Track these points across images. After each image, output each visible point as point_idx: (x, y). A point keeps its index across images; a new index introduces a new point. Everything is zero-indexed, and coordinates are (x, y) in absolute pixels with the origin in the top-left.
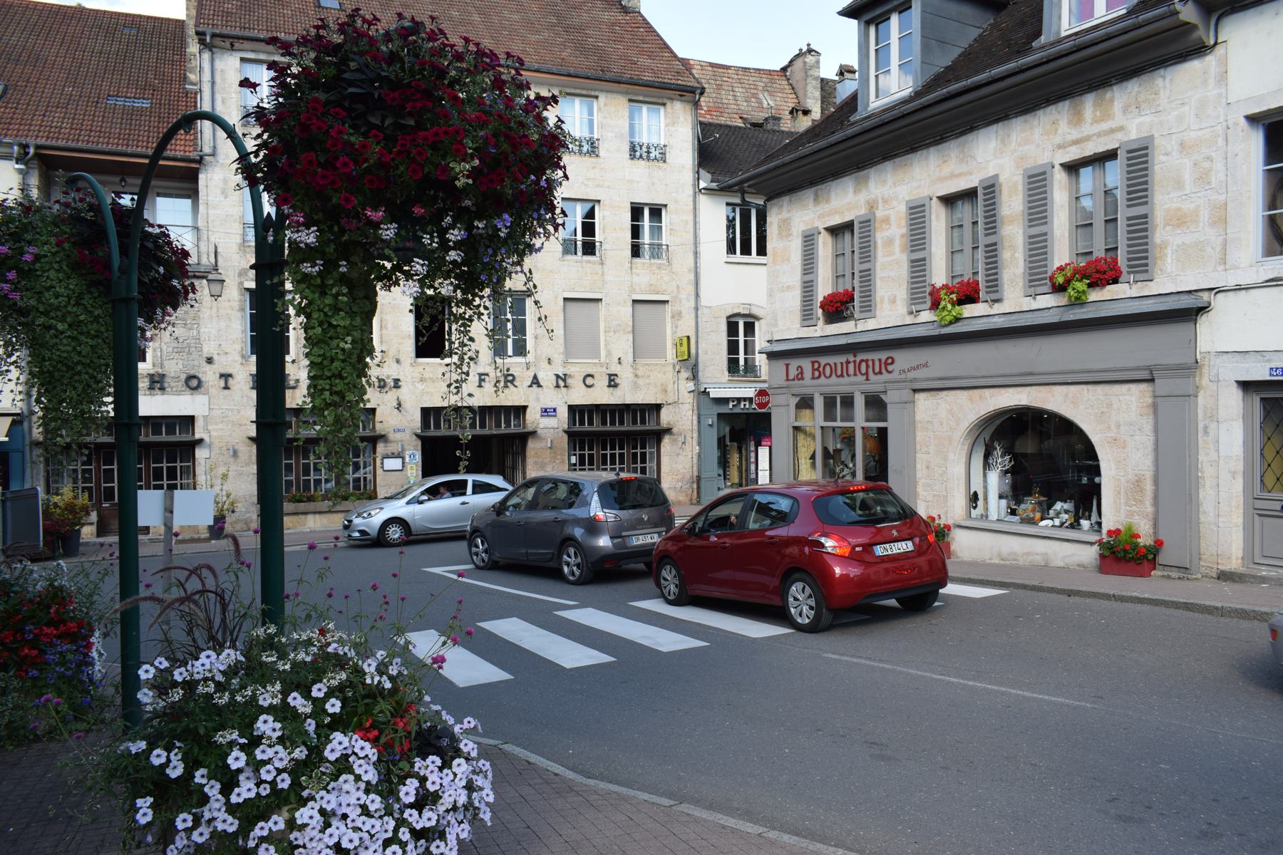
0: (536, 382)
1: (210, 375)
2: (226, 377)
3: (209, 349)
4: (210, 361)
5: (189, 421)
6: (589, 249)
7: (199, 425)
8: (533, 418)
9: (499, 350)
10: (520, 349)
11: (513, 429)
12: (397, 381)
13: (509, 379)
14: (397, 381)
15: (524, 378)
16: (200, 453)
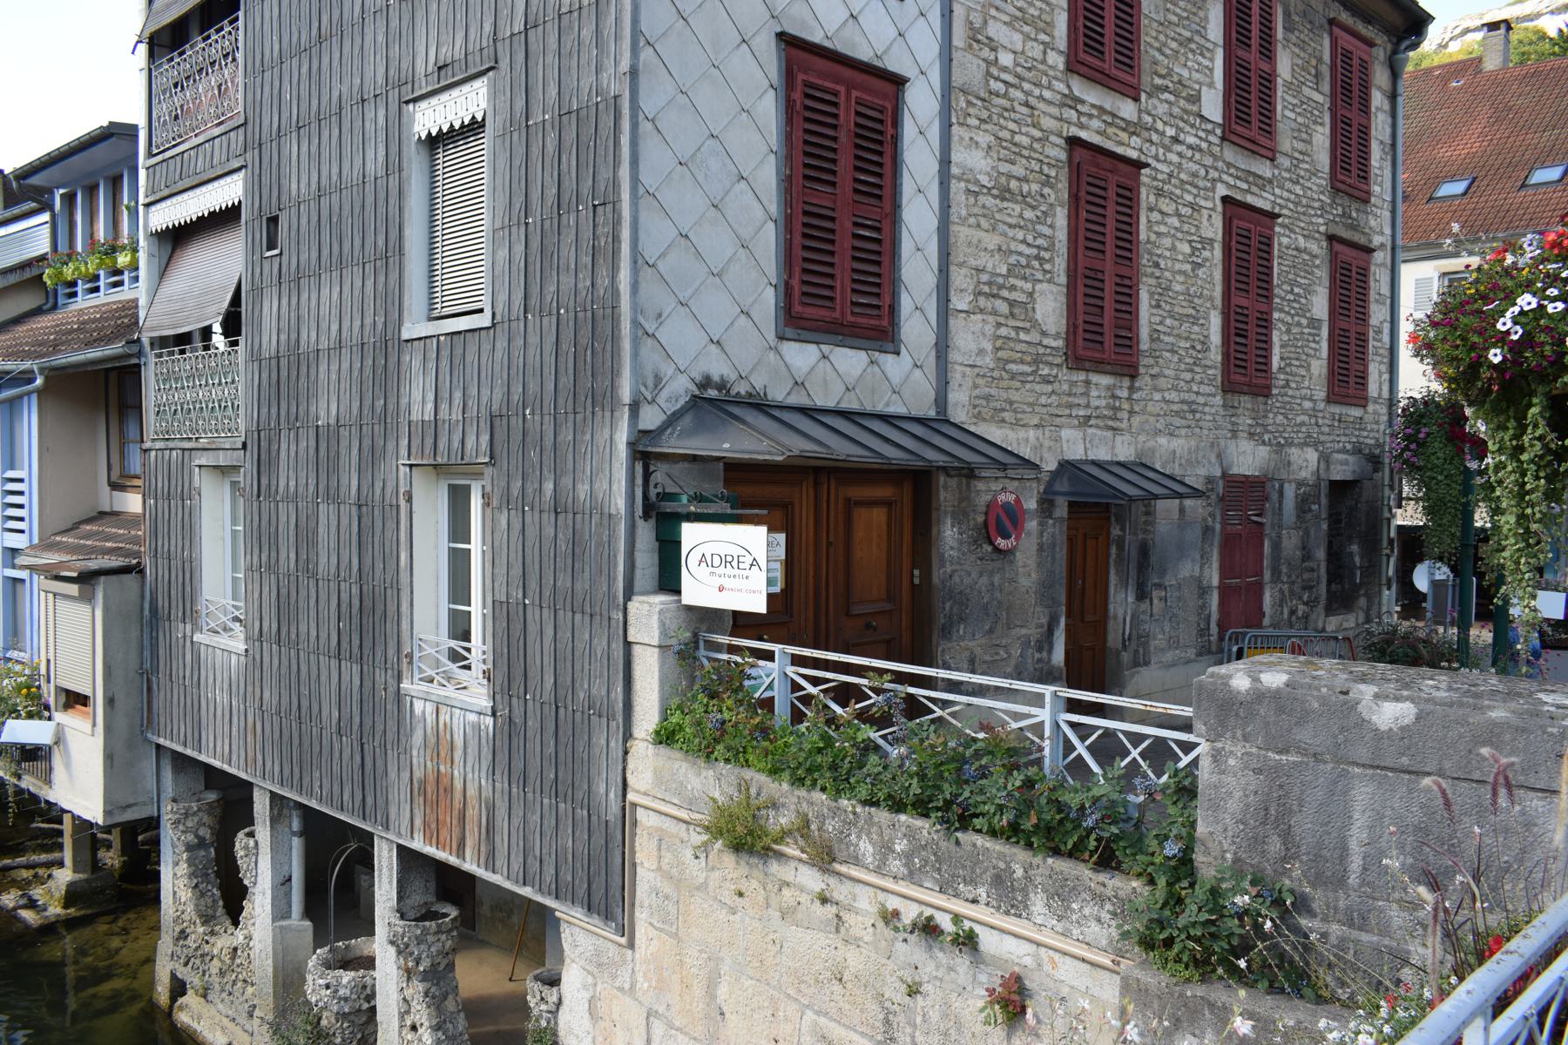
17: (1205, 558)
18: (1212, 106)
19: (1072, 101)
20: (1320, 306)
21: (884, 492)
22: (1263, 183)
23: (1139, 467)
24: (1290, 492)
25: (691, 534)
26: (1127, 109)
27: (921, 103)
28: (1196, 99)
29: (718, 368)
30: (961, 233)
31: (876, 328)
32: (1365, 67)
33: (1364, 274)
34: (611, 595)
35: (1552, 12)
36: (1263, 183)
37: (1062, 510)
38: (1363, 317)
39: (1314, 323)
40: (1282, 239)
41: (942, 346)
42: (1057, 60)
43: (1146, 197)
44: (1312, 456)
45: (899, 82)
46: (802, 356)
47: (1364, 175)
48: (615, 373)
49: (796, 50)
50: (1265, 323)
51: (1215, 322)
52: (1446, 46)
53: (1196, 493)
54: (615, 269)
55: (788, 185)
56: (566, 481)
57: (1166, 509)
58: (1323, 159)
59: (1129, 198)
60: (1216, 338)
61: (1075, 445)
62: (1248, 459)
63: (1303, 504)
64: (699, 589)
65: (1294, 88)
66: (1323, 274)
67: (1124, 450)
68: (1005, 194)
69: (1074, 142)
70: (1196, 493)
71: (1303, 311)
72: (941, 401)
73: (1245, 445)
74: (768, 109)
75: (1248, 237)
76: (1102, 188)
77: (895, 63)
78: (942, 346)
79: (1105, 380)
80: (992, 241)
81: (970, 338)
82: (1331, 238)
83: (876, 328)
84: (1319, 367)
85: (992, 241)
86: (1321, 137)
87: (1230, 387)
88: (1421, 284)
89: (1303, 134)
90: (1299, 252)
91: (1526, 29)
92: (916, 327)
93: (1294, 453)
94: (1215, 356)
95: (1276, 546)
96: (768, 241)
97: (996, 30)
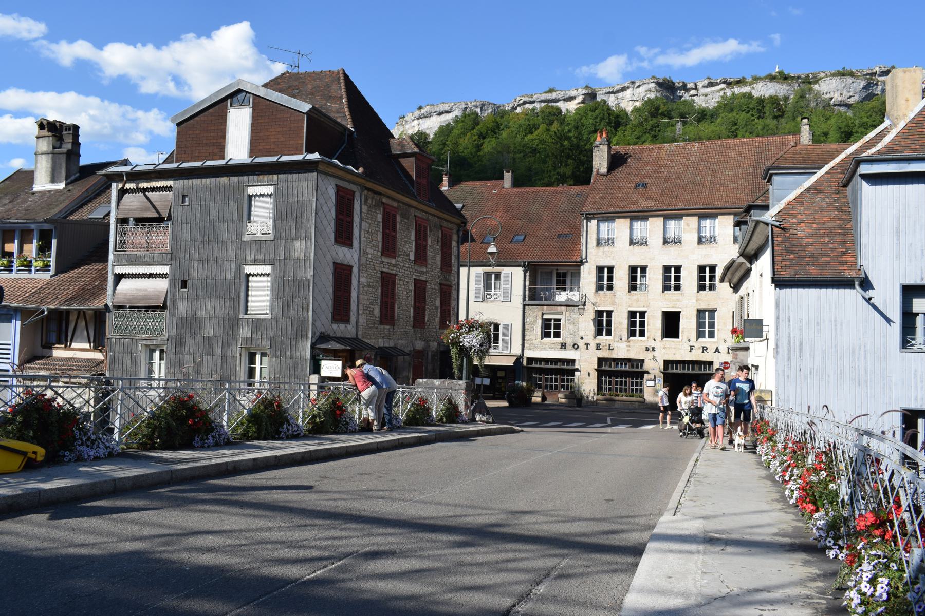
0: (717, 350)
1: (581, 344)
2: (587, 345)
3: (582, 334)
4: (582, 338)
5: (573, 361)
6: (677, 288)
7: (577, 362)
8: (648, 365)
9: (700, 334)
10: (712, 335)
11: (707, 372)
12: (653, 348)
13: (704, 349)
14: (653, 348)
15: (712, 349)
16: (577, 373)
17: (409, 371)
18: (412, 257)
19: (382, 262)
20: (438, 303)
21: (345, 354)
22: (422, 273)
23: (395, 348)
24: (430, 354)
25: (323, 363)
26: (393, 261)
27: (355, 270)
28: (408, 255)
29: (323, 330)
30: (361, 296)
31: (347, 320)
32: (451, 237)
33: (450, 293)
34: (306, 375)
35: (564, 100)
36: (422, 273)
37: (378, 358)
38: (450, 305)
39: (436, 308)
40: (428, 286)
41: (357, 322)
42: (379, 254)
43: (397, 281)
44: (435, 344)
45: (351, 267)
46: (335, 326)
47: (450, 266)
48: (307, 332)
49: (336, 264)
50: (424, 309)
51: (412, 310)
52: (516, 109)
53: (408, 354)
54: (308, 312)
55: (334, 292)
56: (293, 352)
57: (400, 358)
58: (439, 263)
59: (394, 283)
60: (412, 315)
61: (381, 343)
62: (419, 345)
63: (433, 356)
64: (325, 372)
65: (432, 246)
66: (439, 295)
67: (392, 344)
68: (369, 286)
69: (382, 272)
70: (408, 354)
71: (434, 305)
72: (357, 334)
73: (419, 342)
74: (331, 277)
75: (420, 288)
76: (388, 282)
77: (352, 263)
78: (357, 322)
79: (387, 327)
80: (366, 297)
81: (362, 320)
82: (441, 284)
83: (347, 320)
84: (437, 320)
85: (366, 297)
86: (439, 258)
87: (415, 326)
88: (478, 275)
89: (434, 258)
90: (432, 288)
91: (552, 107)
92: (353, 319)
93: (431, 343)
94: (412, 319)
95: (426, 368)
96: (331, 303)
97: (369, 250)
